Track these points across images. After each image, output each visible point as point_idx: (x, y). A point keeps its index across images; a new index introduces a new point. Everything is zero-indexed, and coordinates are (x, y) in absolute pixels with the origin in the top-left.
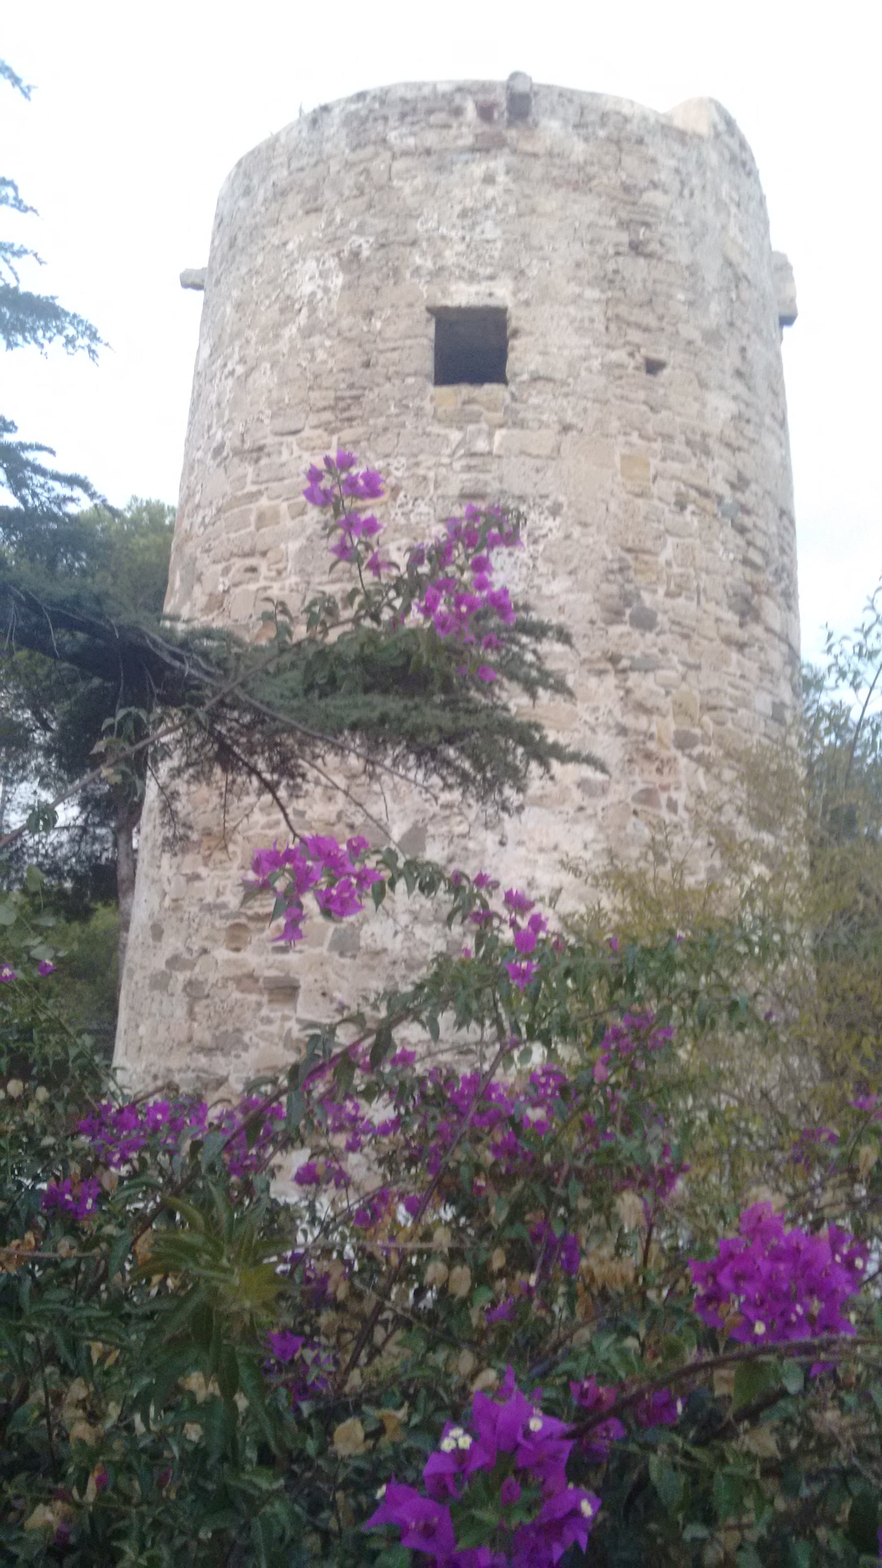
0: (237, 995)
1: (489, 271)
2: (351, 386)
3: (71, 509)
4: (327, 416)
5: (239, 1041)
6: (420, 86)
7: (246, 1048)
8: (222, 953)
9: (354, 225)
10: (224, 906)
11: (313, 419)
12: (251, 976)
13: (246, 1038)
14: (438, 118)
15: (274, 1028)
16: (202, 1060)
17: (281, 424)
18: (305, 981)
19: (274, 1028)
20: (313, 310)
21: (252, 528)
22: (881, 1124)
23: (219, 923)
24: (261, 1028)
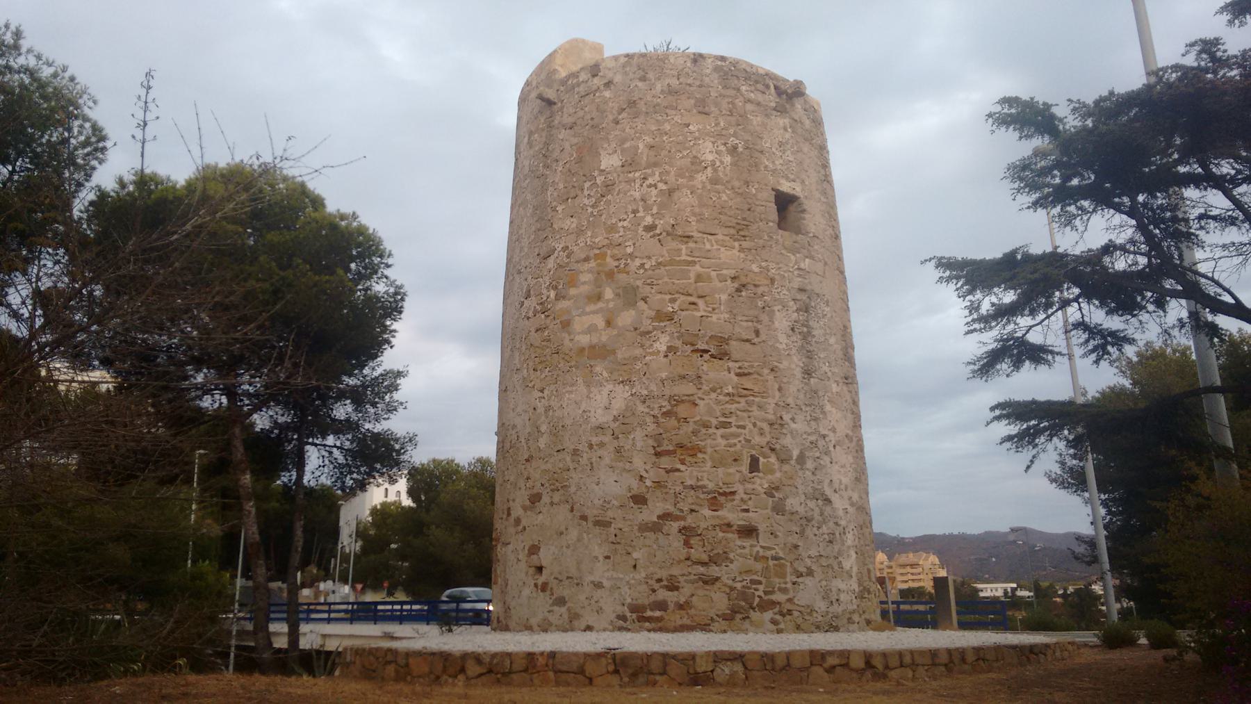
0: (721, 534)
1: (792, 177)
2: (744, 219)
3: (1222, 298)
4: (732, 231)
5: (727, 558)
6: (752, 66)
7: (732, 562)
8: (706, 512)
9: (731, 131)
10: (704, 487)
11: (726, 231)
12: (729, 525)
13: (731, 556)
14: (760, 86)
15: (747, 551)
16: (702, 569)
17: (702, 227)
18: (762, 528)
19: (747, 551)
20: (715, 170)
21: (692, 281)
22: (2, 467)
23: (702, 496)
24: (739, 551)
